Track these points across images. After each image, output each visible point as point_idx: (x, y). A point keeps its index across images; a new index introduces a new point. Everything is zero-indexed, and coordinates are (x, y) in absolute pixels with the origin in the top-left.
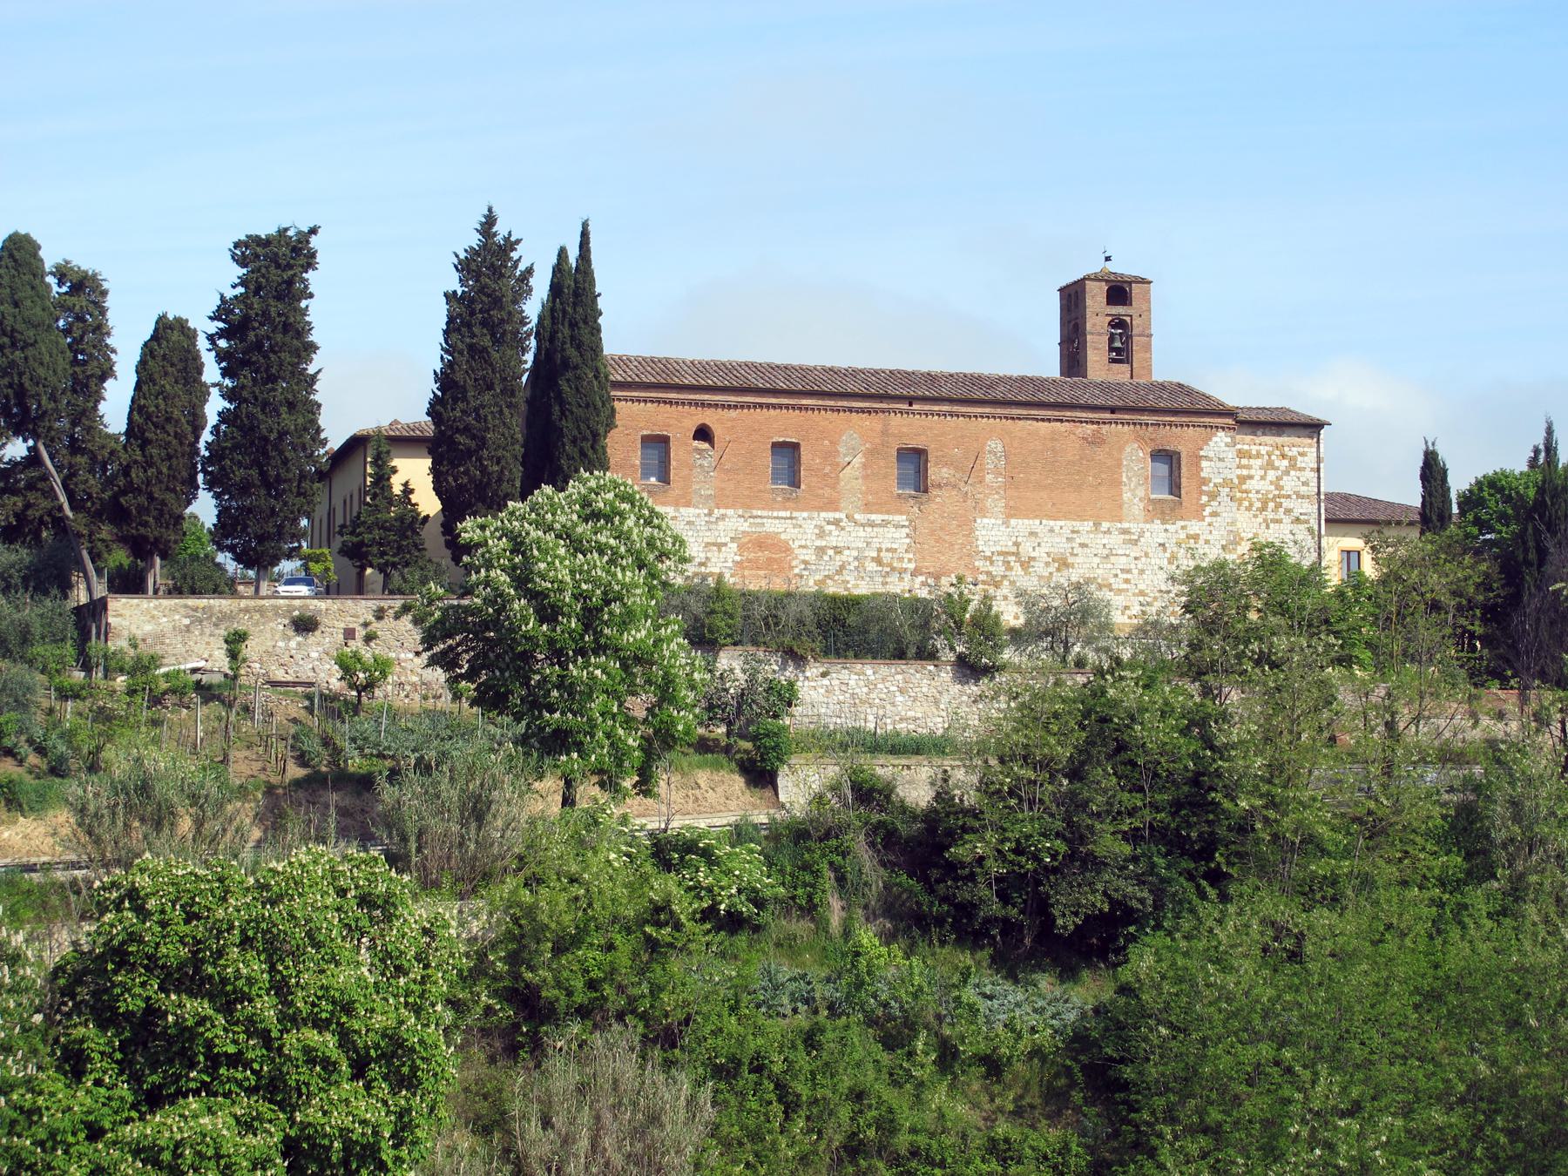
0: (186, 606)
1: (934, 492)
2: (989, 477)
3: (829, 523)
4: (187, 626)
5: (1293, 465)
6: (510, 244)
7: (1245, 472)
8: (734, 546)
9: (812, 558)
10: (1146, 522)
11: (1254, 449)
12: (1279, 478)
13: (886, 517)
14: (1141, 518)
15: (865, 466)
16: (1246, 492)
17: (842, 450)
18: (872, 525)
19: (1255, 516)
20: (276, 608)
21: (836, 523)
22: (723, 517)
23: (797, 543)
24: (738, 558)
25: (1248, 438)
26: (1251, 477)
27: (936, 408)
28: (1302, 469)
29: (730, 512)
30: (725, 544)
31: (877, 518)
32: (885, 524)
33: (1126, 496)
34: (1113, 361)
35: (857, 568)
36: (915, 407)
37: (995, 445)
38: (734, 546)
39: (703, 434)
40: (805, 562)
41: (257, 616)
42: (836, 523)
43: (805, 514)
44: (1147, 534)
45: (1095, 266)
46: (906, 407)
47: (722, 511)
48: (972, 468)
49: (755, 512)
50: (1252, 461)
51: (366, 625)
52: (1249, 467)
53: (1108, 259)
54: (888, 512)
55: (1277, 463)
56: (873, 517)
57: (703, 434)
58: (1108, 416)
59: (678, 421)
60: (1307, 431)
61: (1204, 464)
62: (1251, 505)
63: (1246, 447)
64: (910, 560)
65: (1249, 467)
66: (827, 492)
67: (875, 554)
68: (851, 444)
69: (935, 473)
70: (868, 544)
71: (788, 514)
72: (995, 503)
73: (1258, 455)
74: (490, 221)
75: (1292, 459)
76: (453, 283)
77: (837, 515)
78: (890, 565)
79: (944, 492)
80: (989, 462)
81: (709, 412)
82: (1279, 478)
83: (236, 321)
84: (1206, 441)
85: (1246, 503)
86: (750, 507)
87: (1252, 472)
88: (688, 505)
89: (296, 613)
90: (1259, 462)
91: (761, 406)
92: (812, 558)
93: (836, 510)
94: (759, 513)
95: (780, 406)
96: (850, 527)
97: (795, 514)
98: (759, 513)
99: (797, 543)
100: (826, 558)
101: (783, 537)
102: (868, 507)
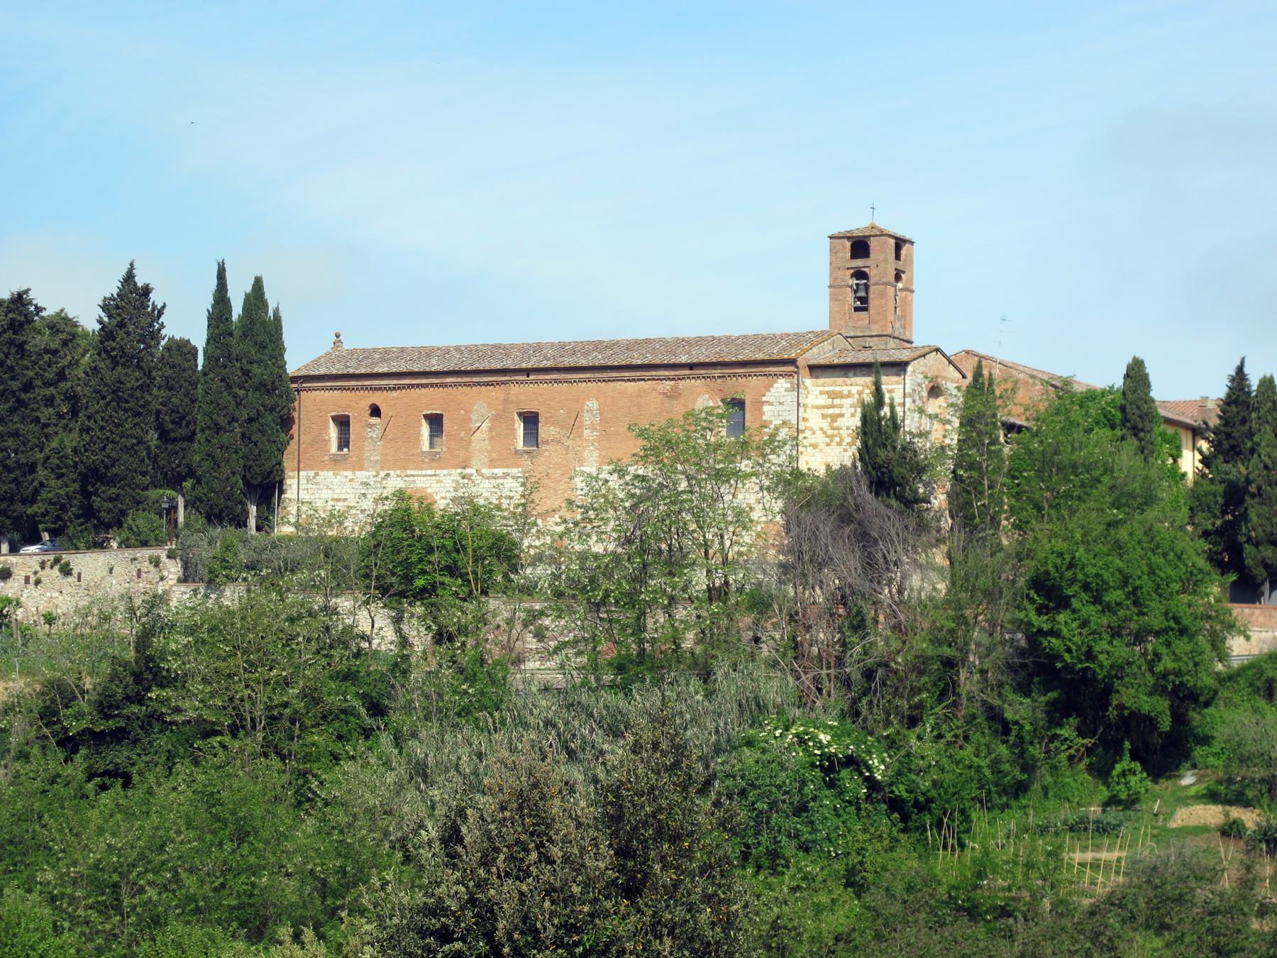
1: (542, 447)
2: (587, 432)
6: (146, 291)
7: (837, 411)
11: (845, 390)
13: (506, 470)
15: (491, 430)
16: (839, 429)
17: (474, 417)
18: (495, 477)
19: (845, 450)
25: (841, 380)
26: (842, 415)
27: (548, 377)
29: (392, 473)
31: (499, 471)
32: (506, 475)
34: (856, 309)
36: (531, 377)
37: (592, 404)
39: (375, 411)
43: (446, 472)
46: (524, 378)
48: (574, 425)
49: (409, 472)
50: (844, 401)
51: (35, 573)
52: (840, 406)
54: (508, 466)
57: (375, 411)
58: (687, 372)
59: (355, 403)
60: (895, 370)
61: (766, 408)
62: (842, 440)
63: (838, 389)
65: (840, 406)
66: (462, 453)
68: (479, 409)
69: (544, 431)
71: (432, 472)
73: (849, 395)
74: (129, 277)
79: (551, 447)
80: (587, 419)
81: (378, 393)
84: (768, 388)
85: (837, 439)
86: (405, 468)
87: (844, 410)
88: (361, 469)
90: (850, 401)
91: (413, 386)
94: (412, 472)
95: (432, 385)
96: (478, 479)
98: (412, 472)
101: (429, 491)
102: (492, 463)
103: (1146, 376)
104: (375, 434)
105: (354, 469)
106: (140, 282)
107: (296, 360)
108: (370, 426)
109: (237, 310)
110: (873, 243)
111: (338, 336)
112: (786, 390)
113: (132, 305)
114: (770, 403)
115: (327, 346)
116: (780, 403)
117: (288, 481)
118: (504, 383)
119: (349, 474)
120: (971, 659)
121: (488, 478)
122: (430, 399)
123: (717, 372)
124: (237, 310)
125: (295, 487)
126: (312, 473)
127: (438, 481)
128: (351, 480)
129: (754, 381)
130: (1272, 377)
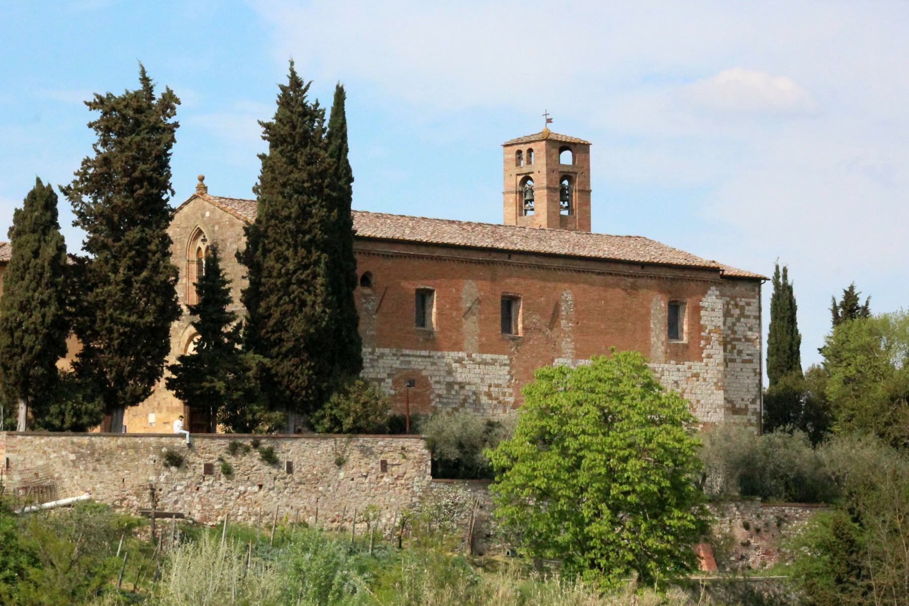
0: (73, 443)
2: (563, 322)
3: (456, 362)
4: (73, 461)
5: (742, 315)
8: (389, 381)
9: (443, 392)
10: (666, 362)
12: (734, 324)
13: (495, 356)
14: (663, 359)
20: (147, 446)
21: (460, 361)
22: (382, 356)
23: (434, 379)
24: (392, 392)
28: (748, 317)
29: (387, 351)
30: (383, 380)
31: (488, 357)
32: (493, 363)
33: (653, 340)
35: (474, 401)
38: (389, 381)
40: (439, 396)
41: (131, 452)
42: (460, 361)
44: (666, 373)
45: (536, 127)
47: (382, 350)
53: (549, 121)
54: (495, 353)
55: (733, 312)
56: (484, 356)
64: (511, 395)
67: (486, 389)
70: (482, 380)
72: (567, 345)
75: (742, 309)
76: (265, 148)
77: (461, 354)
78: (497, 399)
82: (734, 324)
83: (96, 178)
89: (164, 450)
92: (443, 392)
93: (460, 350)
96: (470, 366)
97: (432, 353)
98: (407, 352)
99: (434, 379)
100: (453, 392)
101: (424, 373)
102: (482, 349)
103: (348, 170)
106: (45, 185)
121: (479, 364)
127: (433, 364)
130: (100, 103)
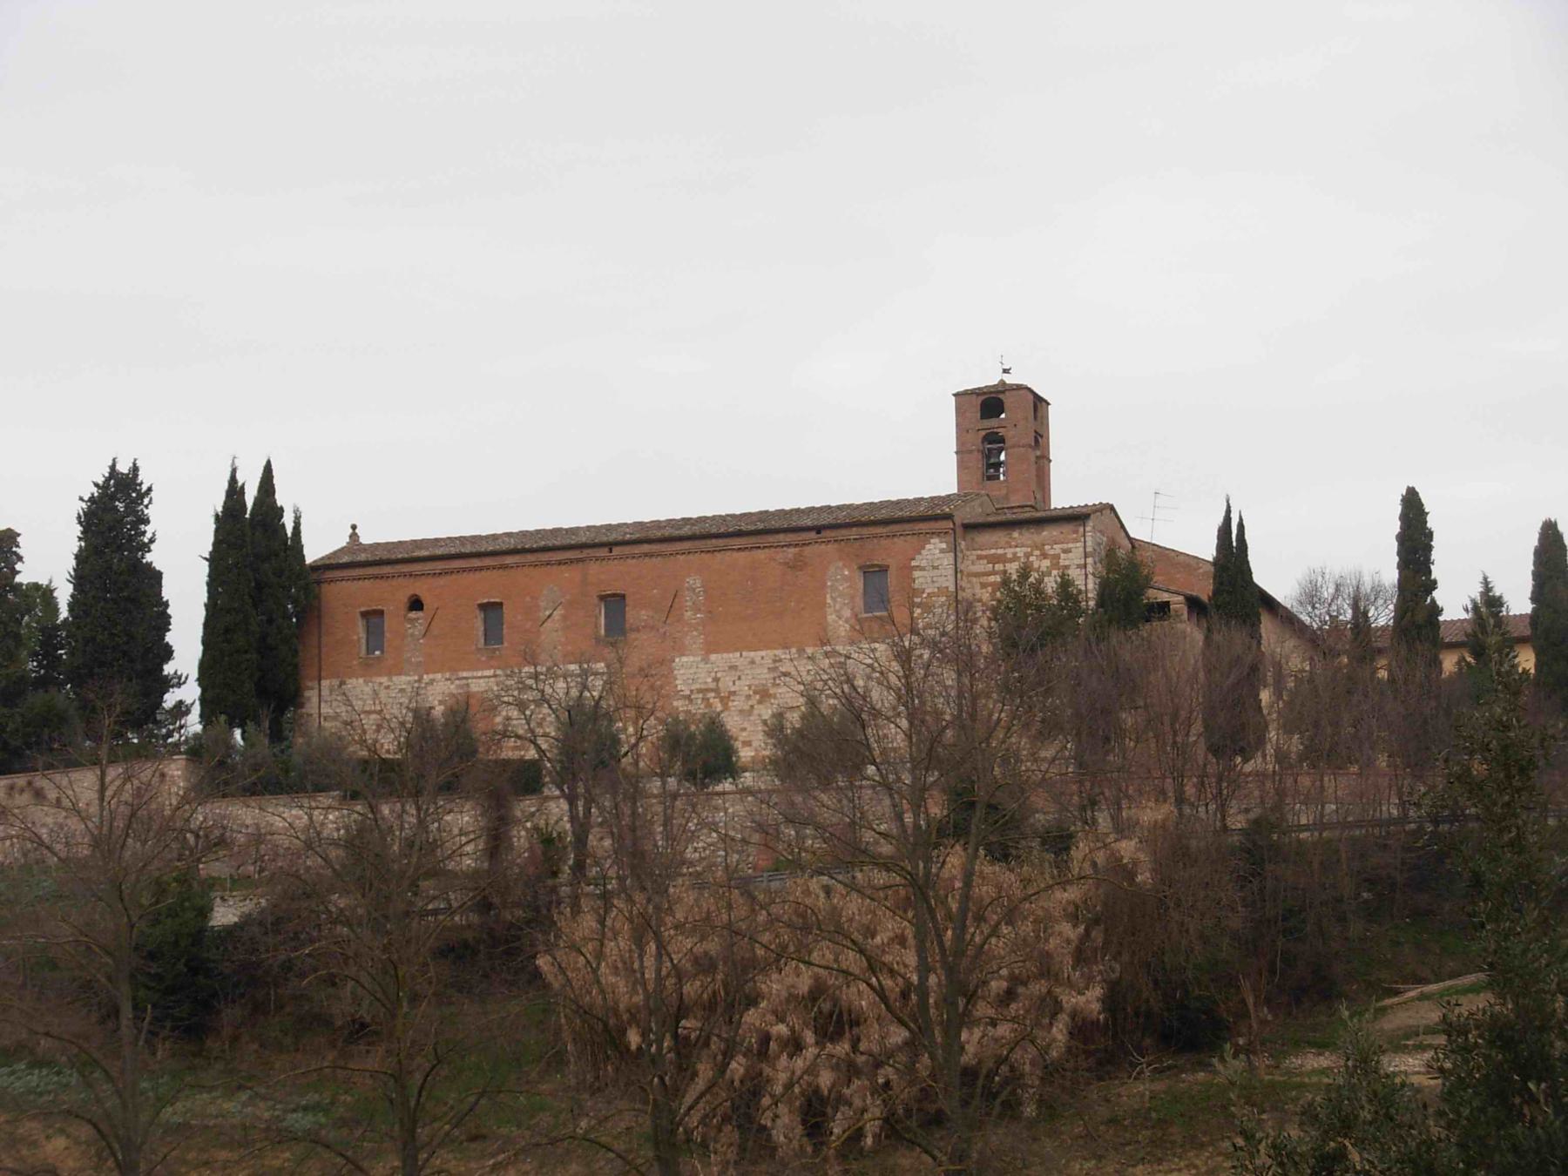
11: (1009, 552)
15: (565, 618)
29: (439, 676)
37: (695, 581)
39: (416, 604)
48: (672, 608)
57: (416, 604)
63: (1000, 551)
69: (636, 615)
91: (464, 570)
104: (419, 629)
105: (390, 674)
107: (314, 550)
108: (412, 621)
109: (250, 499)
110: (1008, 399)
111: (354, 527)
112: (942, 551)
113: (20, 559)
114: (918, 568)
115: (342, 541)
116: (935, 568)
117: (307, 694)
118: (579, 560)
119: (384, 680)
120: (607, 843)
122: (487, 585)
123: (853, 533)
124: (250, 499)
125: (315, 700)
126: (336, 682)
128: (387, 687)
129: (899, 542)
